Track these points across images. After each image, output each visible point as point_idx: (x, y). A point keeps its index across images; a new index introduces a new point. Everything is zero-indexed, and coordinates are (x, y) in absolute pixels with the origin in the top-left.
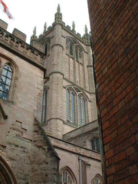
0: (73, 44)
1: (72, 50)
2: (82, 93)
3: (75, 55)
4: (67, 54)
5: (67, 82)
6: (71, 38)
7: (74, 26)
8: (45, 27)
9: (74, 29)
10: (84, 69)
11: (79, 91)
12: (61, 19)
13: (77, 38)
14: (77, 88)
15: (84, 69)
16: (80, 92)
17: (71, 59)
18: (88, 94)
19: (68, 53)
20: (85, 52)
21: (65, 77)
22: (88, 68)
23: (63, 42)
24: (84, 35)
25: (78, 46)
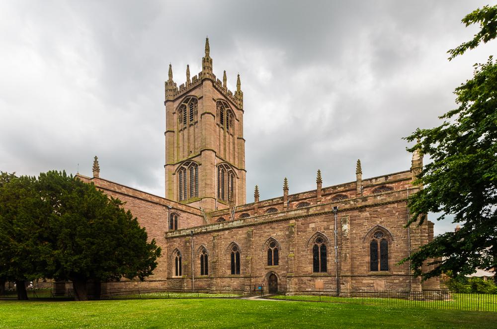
4: (217, 124)
6: (222, 101)
7: (225, 80)
8: (188, 74)
10: (234, 140)
11: (228, 168)
13: (230, 101)
15: (234, 140)
17: (222, 131)
18: (236, 171)
20: (237, 119)
22: (145, 281)
23: (213, 107)
24: (236, 92)
25: (229, 110)
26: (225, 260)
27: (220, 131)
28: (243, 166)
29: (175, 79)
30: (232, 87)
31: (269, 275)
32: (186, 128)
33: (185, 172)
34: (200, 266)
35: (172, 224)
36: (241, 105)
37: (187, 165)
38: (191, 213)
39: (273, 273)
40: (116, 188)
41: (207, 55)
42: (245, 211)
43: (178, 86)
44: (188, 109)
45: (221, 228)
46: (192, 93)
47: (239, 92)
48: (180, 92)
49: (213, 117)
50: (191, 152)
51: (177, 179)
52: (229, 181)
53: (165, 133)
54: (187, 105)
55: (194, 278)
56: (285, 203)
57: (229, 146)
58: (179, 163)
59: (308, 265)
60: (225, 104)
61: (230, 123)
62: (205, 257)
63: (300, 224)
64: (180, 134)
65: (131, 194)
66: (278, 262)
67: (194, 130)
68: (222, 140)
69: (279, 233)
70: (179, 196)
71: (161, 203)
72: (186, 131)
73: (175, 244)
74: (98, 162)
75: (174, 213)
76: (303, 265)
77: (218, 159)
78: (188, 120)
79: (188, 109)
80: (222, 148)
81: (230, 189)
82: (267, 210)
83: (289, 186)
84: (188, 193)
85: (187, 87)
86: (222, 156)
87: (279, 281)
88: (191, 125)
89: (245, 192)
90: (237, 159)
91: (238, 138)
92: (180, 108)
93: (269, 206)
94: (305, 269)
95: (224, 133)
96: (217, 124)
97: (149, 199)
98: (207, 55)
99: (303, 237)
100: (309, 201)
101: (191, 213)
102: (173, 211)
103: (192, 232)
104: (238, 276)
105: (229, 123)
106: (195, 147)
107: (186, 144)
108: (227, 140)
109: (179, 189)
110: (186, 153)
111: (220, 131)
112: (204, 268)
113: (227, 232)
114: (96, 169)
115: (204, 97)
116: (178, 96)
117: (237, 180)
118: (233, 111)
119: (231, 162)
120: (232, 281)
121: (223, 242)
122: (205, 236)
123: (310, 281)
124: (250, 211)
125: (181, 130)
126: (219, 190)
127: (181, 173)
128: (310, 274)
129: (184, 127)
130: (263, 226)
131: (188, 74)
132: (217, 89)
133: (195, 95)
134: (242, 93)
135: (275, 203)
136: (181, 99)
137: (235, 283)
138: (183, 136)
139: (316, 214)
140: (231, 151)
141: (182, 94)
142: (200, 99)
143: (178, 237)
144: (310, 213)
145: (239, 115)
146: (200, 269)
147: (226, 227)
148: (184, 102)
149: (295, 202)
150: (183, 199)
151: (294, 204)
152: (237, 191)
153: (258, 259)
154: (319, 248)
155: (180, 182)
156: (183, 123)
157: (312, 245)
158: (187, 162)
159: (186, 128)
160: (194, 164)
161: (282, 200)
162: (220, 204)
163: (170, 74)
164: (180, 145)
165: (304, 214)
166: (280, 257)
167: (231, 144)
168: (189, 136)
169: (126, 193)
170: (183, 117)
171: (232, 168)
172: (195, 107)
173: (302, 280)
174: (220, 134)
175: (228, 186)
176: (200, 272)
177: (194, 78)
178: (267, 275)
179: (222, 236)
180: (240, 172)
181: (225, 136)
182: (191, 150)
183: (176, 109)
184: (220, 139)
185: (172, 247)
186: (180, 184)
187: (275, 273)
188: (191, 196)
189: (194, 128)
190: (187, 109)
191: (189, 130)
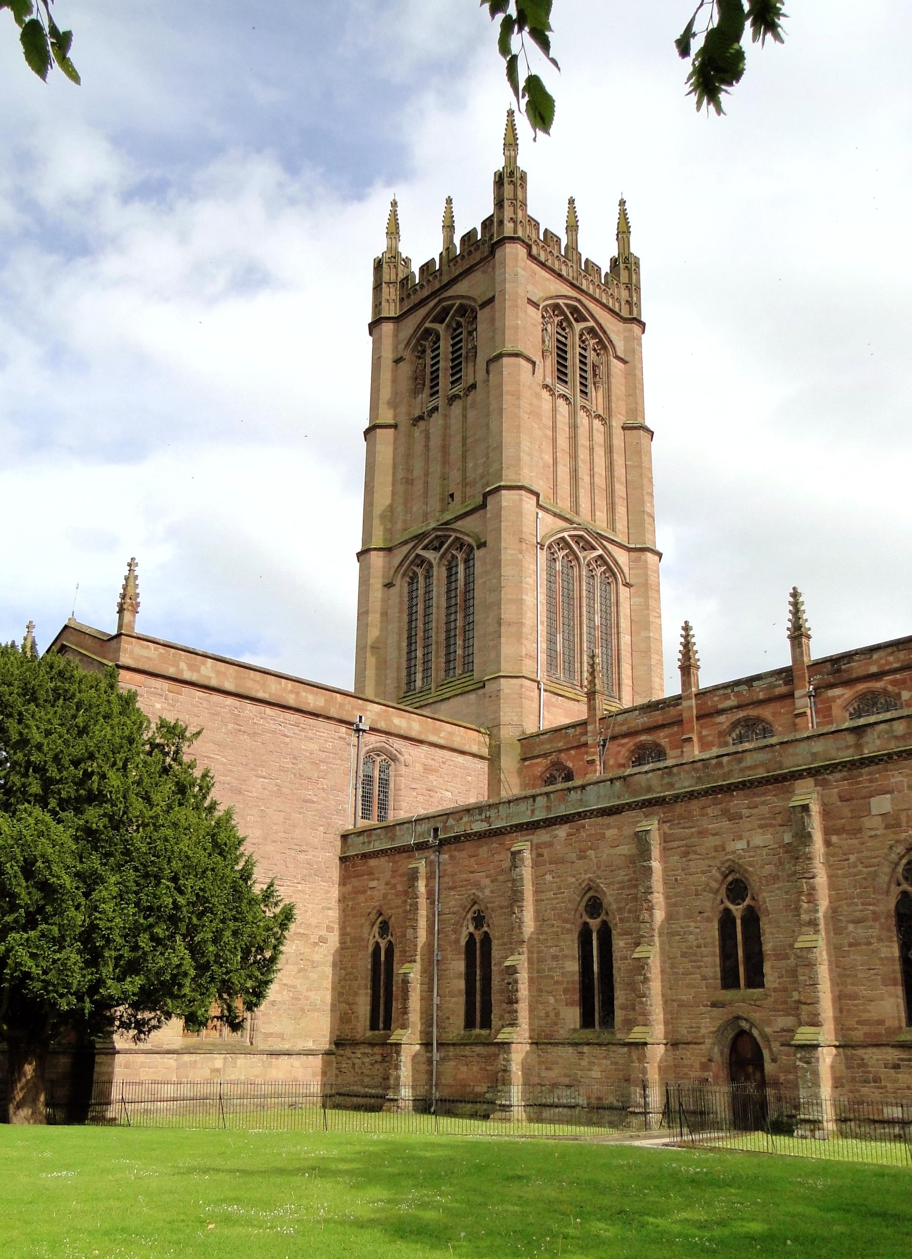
0: (570, 325)
1: (558, 340)
2: (600, 556)
3: (578, 372)
4: (546, 386)
5: (517, 396)
6: (561, 302)
7: (572, 227)
8: (449, 227)
9: (572, 247)
10: (609, 435)
12: (524, 204)
14: (581, 537)
15: (609, 435)
16: (594, 548)
17: (561, 402)
18: (622, 557)
19: (549, 381)
21: (535, 498)
24: (614, 263)
25: (591, 330)
26: (555, 958)
27: (554, 410)
28: (648, 536)
29: (404, 250)
30: (598, 248)
31: (731, 1035)
32: (436, 409)
33: (428, 577)
34: (461, 984)
35: (367, 798)
36: (633, 304)
37: (437, 549)
38: (442, 747)
39: (744, 1025)
40: (183, 665)
41: (511, 160)
42: (649, 730)
43: (415, 268)
44: (445, 346)
45: (540, 815)
46: (462, 288)
47: (627, 260)
48: (422, 287)
49: (530, 366)
50: (452, 496)
51: (401, 603)
52: (591, 598)
53: (367, 432)
54: (440, 328)
55: (440, 1045)
56: (798, 693)
57: (592, 463)
58: (405, 543)
59: (883, 990)
60: (574, 310)
61: (595, 375)
62: (482, 941)
63: (835, 799)
64: (417, 433)
65: (229, 686)
66: (763, 975)
67: (464, 416)
68: (563, 442)
69: (759, 839)
70: (404, 673)
71: (333, 713)
72: (437, 420)
73: (374, 884)
74: (136, 577)
75: (379, 751)
76: (863, 991)
77: (549, 519)
78: (444, 380)
79: (445, 346)
80: (564, 471)
81: (598, 634)
82: (734, 725)
83: (811, 620)
84: (438, 661)
85: (445, 268)
86: (564, 505)
87: (769, 1067)
88: (452, 399)
89: (660, 641)
90: (621, 510)
91: (624, 428)
92: (418, 340)
93: (739, 707)
94: (871, 1007)
95: (573, 415)
96: (546, 386)
97: (291, 701)
98: (511, 160)
99: (852, 858)
100: (894, 683)
101: (442, 747)
102: (373, 740)
103: (436, 830)
104: (606, 1037)
105: (589, 375)
106: (464, 478)
107: (436, 468)
108: (583, 440)
109: (405, 644)
110: (435, 503)
111: (554, 410)
112: (478, 998)
113: (562, 832)
114: (127, 603)
115: (496, 300)
116: (415, 299)
117: (624, 592)
118: (605, 332)
119: (601, 524)
120: (584, 1063)
121: (548, 877)
122: (483, 851)
123: (896, 1067)
124: (667, 731)
125: (421, 418)
126: (551, 641)
127: (413, 579)
128: (891, 1032)
129: (431, 405)
130: (695, 805)
131: (449, 227)
132: (543, 265)
133: (469, 294)
134: (637, 259)
135: (761, 696)
136: (423, 312)
137: (596, 1073)
138: (427, 438)
139: (890, 756)
140: (600, 481)
141: (426, 293)
142: (484, 305)
143: (384, 852)
144: (867, 752)
145: (627, 340)
146: (462, 999)
147: (562, 811)
148: (432, 322)
149: (837, 692)
150: (419, 683)
151: (834, 699)
152: (626, 639)
153: (684, 955)
154: (595, 936)
155: (410, 614)
156: (427, 391)
157: (888, 892)
158: (437, 540)
159: (436, 409)
160: (460, 544)
161: (786, 684)
162: (554, 698)
163: (393, 231)
164: (415, 474)
165: (847, 755)
166: (768, 946)
167: (600, 452)
168: (445, 437)
169: (214, 683)
170: (428, 370)
171: (604, 548)
172: (470, 333)
173: (863, 1065)
174: (554, 422)
175: (591, 620)
176: (461, 1010)
177: (468, 238)
178: (722, 1030)
179: (545, 852)
180: (638, 560)
181: (574, 427)
182: (452, 488)
183: (408, 344)
184: (554, 440)
185: (361, 898)
186: (410, 622)
187: (752, 1025)
188: (447, 671)
189: (465, 409)
190: (442, 343)
191: (446, 416)
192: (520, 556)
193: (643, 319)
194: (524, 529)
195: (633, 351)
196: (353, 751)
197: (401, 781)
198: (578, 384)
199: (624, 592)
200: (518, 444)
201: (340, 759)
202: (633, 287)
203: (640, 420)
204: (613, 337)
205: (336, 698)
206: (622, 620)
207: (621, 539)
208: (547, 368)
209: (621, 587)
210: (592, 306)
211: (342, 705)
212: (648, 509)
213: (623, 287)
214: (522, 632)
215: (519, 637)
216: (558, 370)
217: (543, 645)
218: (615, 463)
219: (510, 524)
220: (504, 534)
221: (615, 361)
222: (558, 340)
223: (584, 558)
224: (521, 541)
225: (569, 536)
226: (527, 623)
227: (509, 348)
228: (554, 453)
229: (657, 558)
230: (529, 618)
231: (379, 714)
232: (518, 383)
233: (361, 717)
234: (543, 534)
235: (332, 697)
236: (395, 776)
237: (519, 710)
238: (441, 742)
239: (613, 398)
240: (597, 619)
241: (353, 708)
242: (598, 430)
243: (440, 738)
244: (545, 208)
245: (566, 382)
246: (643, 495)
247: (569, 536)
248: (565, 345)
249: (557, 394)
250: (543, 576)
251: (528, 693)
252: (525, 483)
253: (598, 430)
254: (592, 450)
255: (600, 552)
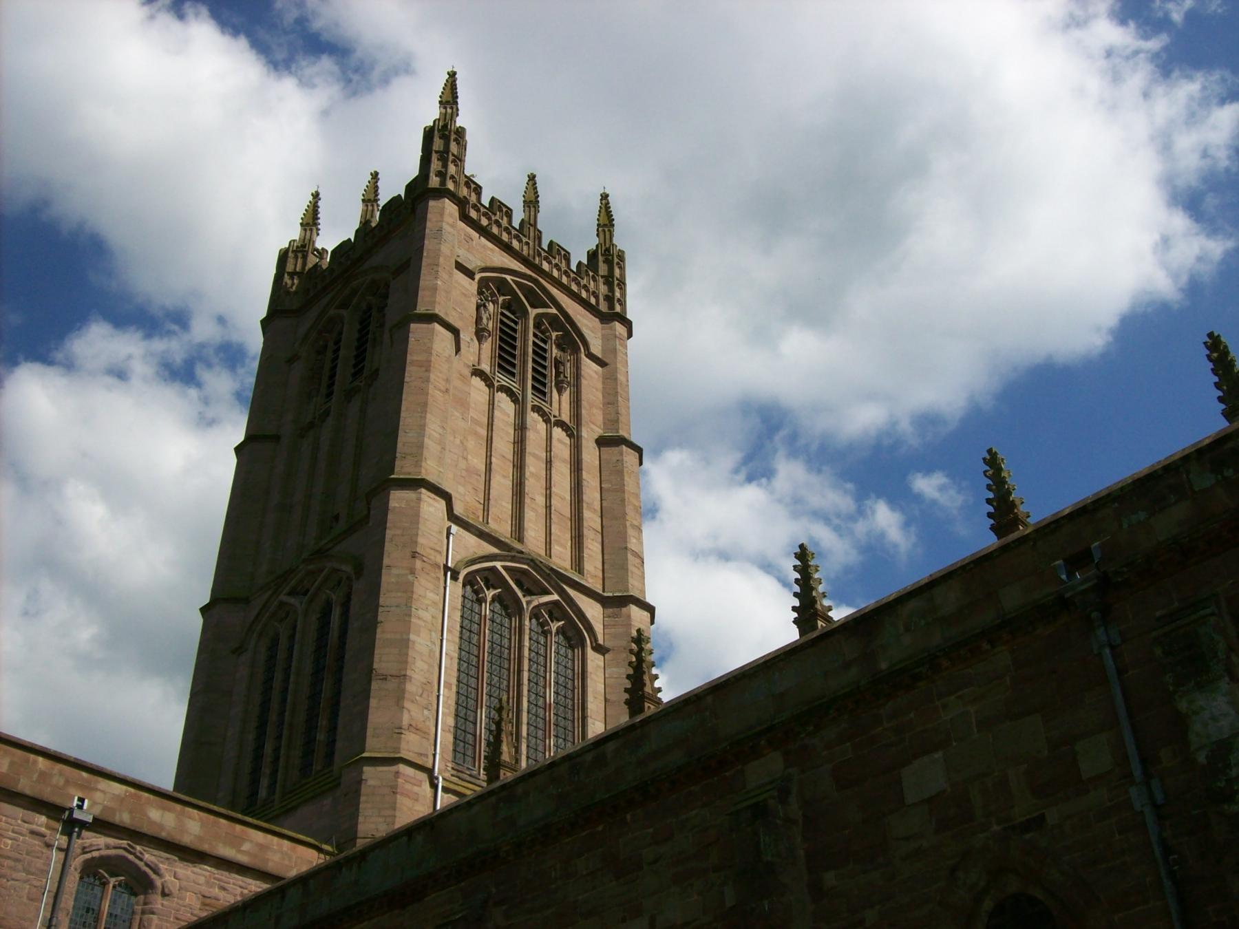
1: (502, 322)
5: (427, 366)
7: (532, 203)
9: (530, 224)
12: (459, 160)
17: (501, 397)
18: (593, 611)
19: (485, 367)
24: (592, 256)
25: (554, 322)
27: (492, 404)
75: (112, 865)
77: (471, 540)
86: (501, 526)
102: (100, 843)
111: (492, 404)
119: (561, 558)
125: (312, 425)
145: (605, 339)
148: (337, 308)
171: (562, 593)
181: (521, 428)
184: (489, 441)
192: (410, 577)
193: (629, 316)
194: (421, 540)
195: (614, 351)
196: (56, 856)
197: (150, 920)
198: (530, 370)
199: (594, 661)
200: (423, 427)
201: (24, 870)
202: (616, 282)
203: (622, 433)
204: (585, 331)
205: (35, 762)
206: (590, 698)
207: (595, 584)
208: (483, 354)
209: (590, 652)
210: (555, 292)
211: (43, 775)
212: (632, 544)
213: (601, 280)
214: (403, 691)
215: (399, 698)
216: (500, 357)
217: (446, 719)
218: (585, 483)
219: (399, 532)
220: (387, 546)
221: (586, 361)
222: (502, 322)
223: (528, 603)
224: (414, 555)
225: (505, 568)
226: (415, 676)
227: (421, 309)
228: (489, 456)
229: (646, 615)
230: (419, 670)
231: (121, 800)
232: (429, 351)
233: (82, 800)
234: (459, 558)
235: (27, 761)
236: (143, 912)
237: (389, 812)
238: (243, 859)
239: (584, 403)
240: (551, 696)
241: (67, 782)
242: (560, 441)
243: (239, 851)
244: (491, 167)
245: (513, 375)
246: (625, 527)
247: (505, 568)
248: (515, 331)
249: (496, 384)
250: (453, 619)
251: (408, 786)
252: (431, 478)
253: (560, 441)
254: (549, 463)
255: (556, 597)
